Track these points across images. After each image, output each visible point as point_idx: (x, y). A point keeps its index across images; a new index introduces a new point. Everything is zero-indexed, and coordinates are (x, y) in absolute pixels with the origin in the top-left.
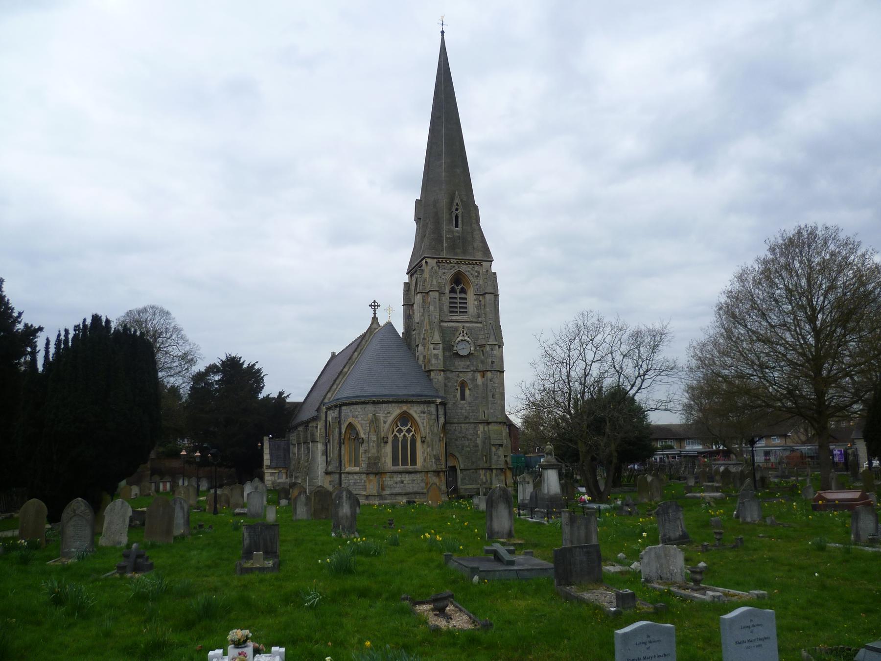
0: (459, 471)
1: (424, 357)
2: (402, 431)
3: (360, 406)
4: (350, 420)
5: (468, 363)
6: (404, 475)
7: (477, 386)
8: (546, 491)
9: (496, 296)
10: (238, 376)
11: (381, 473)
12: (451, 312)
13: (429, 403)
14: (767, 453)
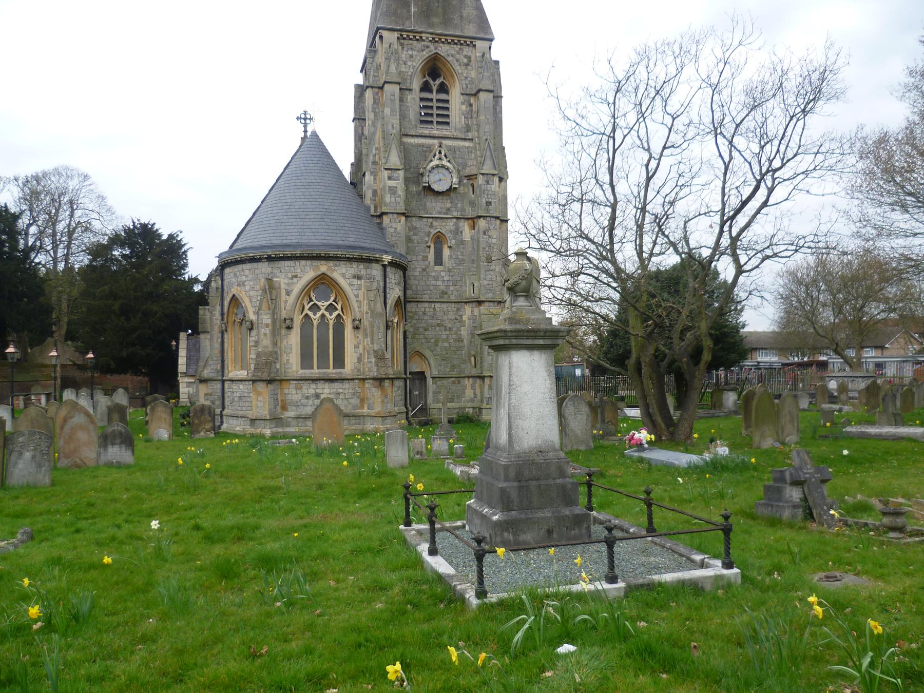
0: (430, 381)
1: (375, 192)
2: (319, 308)
3: (248, 266)
4: (234, 291)
5: (449, 205)
6: (320, 385)
7: (462, 242)
8: (503, 438)
9: (498, 98)
10: (150, 253)
11: (281, 380)
12: (422, 122)
13: (369, 260)
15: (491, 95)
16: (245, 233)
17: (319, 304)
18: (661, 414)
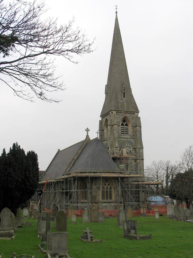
14: (109, 209)
17: (106, 184)
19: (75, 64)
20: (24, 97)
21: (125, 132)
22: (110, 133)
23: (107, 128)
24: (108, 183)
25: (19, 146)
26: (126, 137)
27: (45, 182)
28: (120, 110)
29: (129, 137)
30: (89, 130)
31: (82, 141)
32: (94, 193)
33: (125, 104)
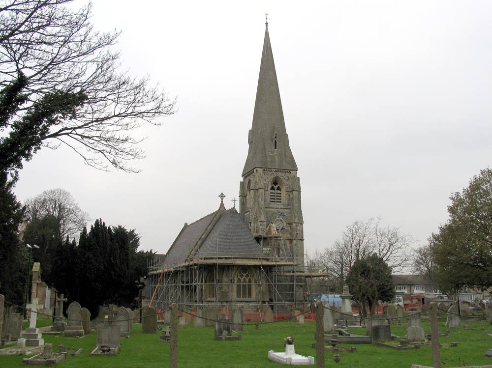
15: (297, 192)
16: (185, 231)
18: (63, 310)
19: (157, 126)
20: (97, 166)
21: (276, 199)
22: (253, 201)
23: (250, 192)
24: (246, 274)
25: (104, 224)
26: (277, 206)
27: (161, 271)
28: (268, 167)
29: (282, 206)
30: (225, 196)
31: (214, 213)
32: (225, 288)
33: (277, 158)
